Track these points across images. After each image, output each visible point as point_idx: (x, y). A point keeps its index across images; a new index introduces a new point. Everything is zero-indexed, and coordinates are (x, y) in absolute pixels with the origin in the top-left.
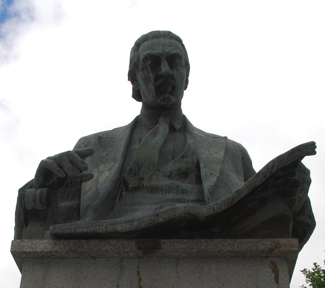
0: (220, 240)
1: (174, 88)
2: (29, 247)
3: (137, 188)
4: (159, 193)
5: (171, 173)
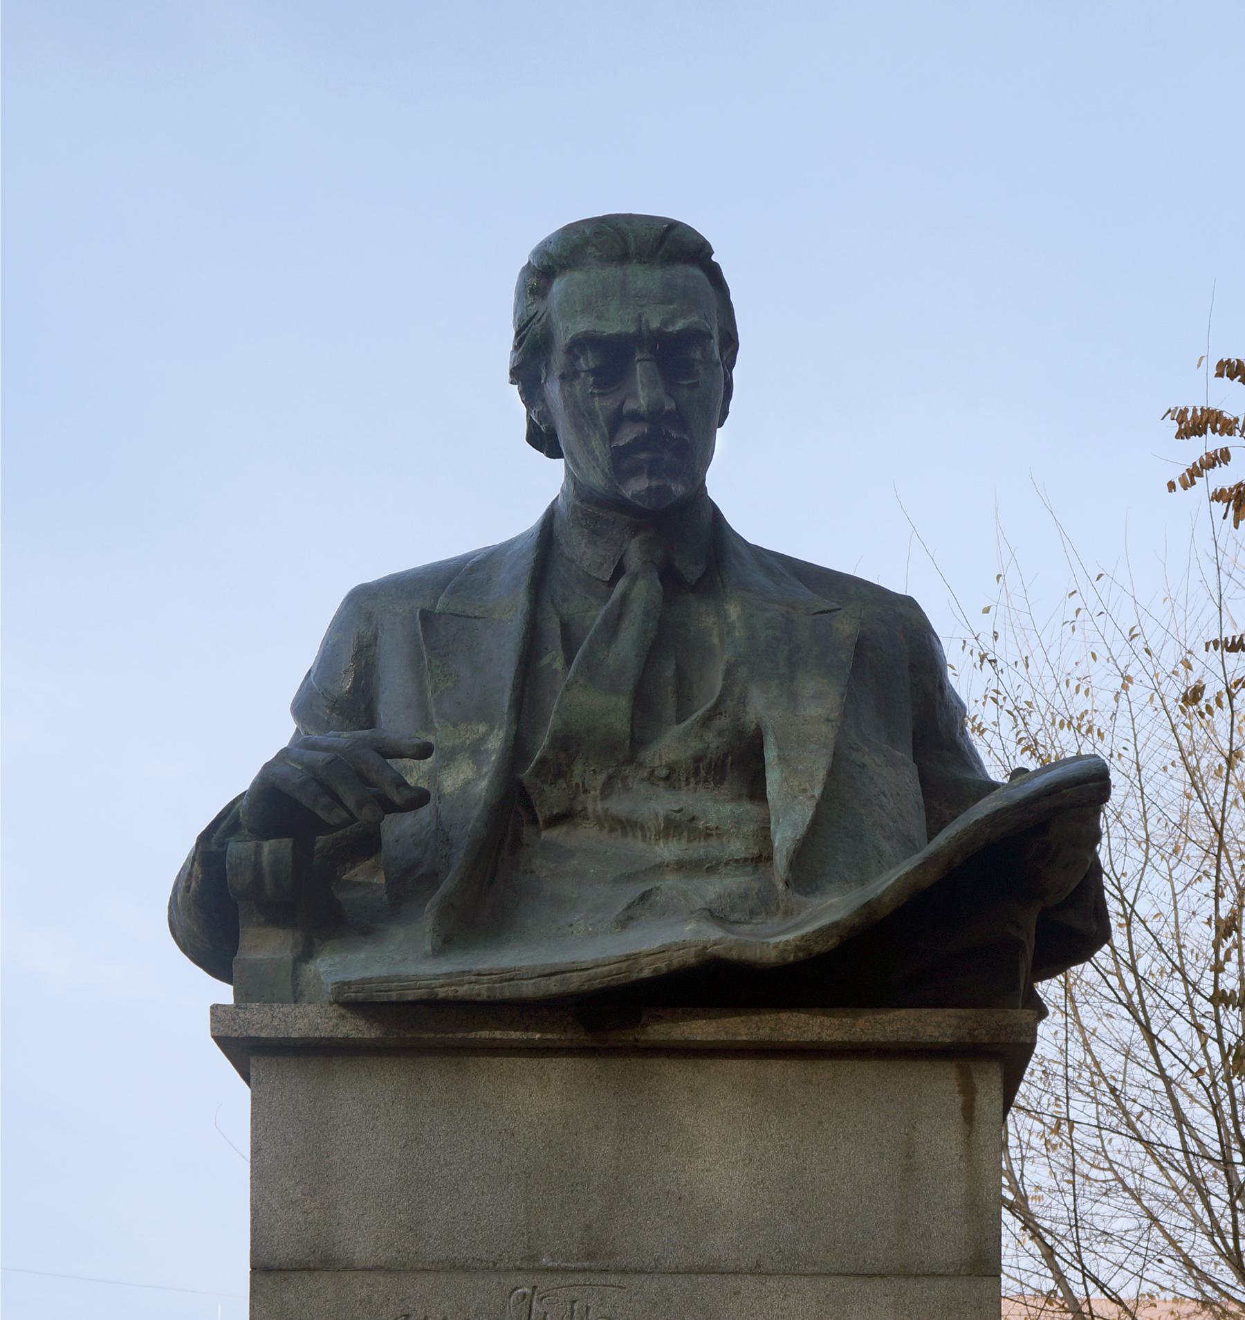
2: (267, 1026)
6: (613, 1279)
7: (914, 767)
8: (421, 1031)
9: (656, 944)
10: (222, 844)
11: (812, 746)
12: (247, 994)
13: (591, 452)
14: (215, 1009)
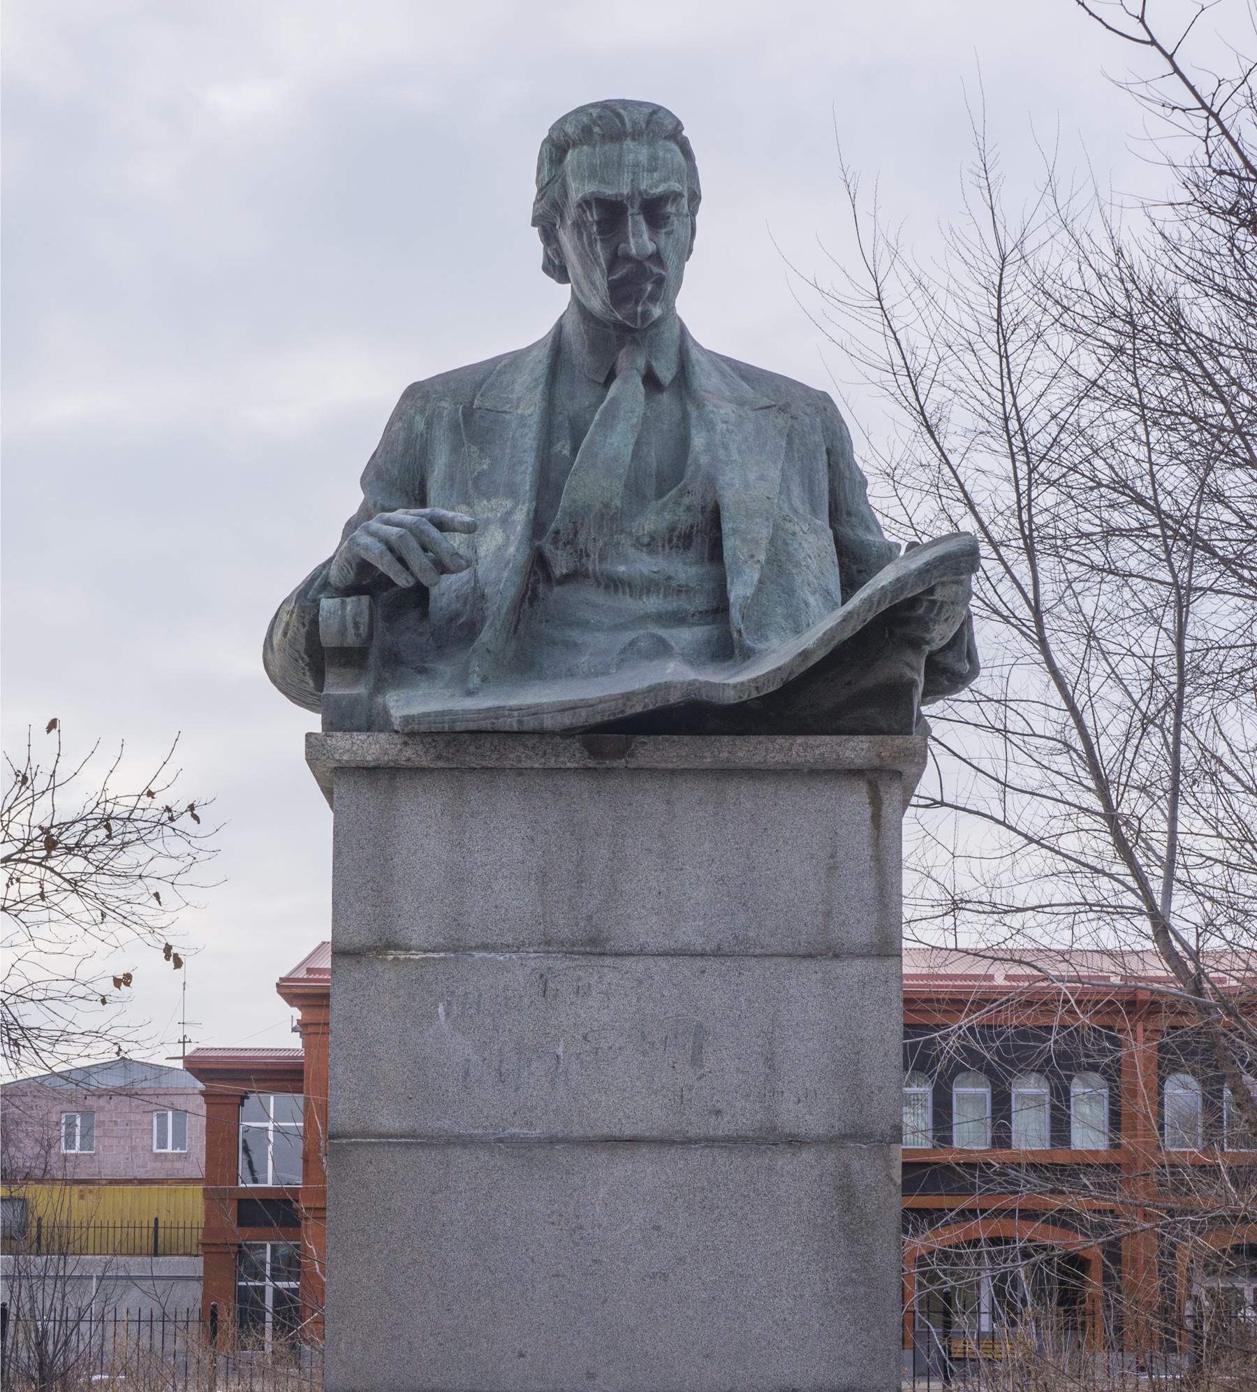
0: (761, 738)
1: (660, 282)
3: (574, 576)
4: (624, 593)
5: (653, 538)
6: (608, 961)
7: (830, 532)
8: (462, 751)
9: (645, 684)
10: (316, 602)
11: (758, 520)
12: (331, 724)
13: (593, 284)
14: (309, 736)
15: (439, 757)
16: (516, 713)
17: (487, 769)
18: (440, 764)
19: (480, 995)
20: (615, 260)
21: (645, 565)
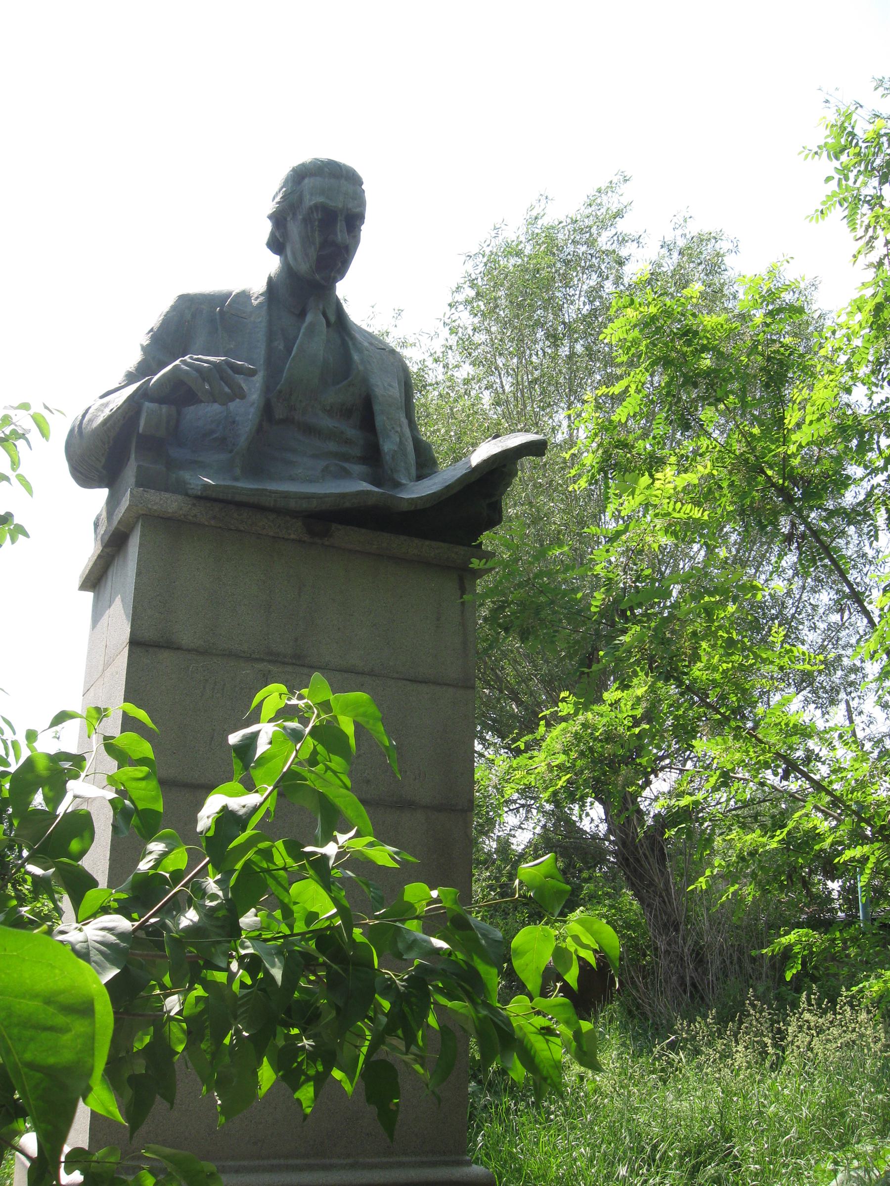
15: (214, 518)
16: (273, 495)
17: (240, 531)
18: (213, 523)
19: (225, 685)
20: (325, 244)
21: (327, 422)
